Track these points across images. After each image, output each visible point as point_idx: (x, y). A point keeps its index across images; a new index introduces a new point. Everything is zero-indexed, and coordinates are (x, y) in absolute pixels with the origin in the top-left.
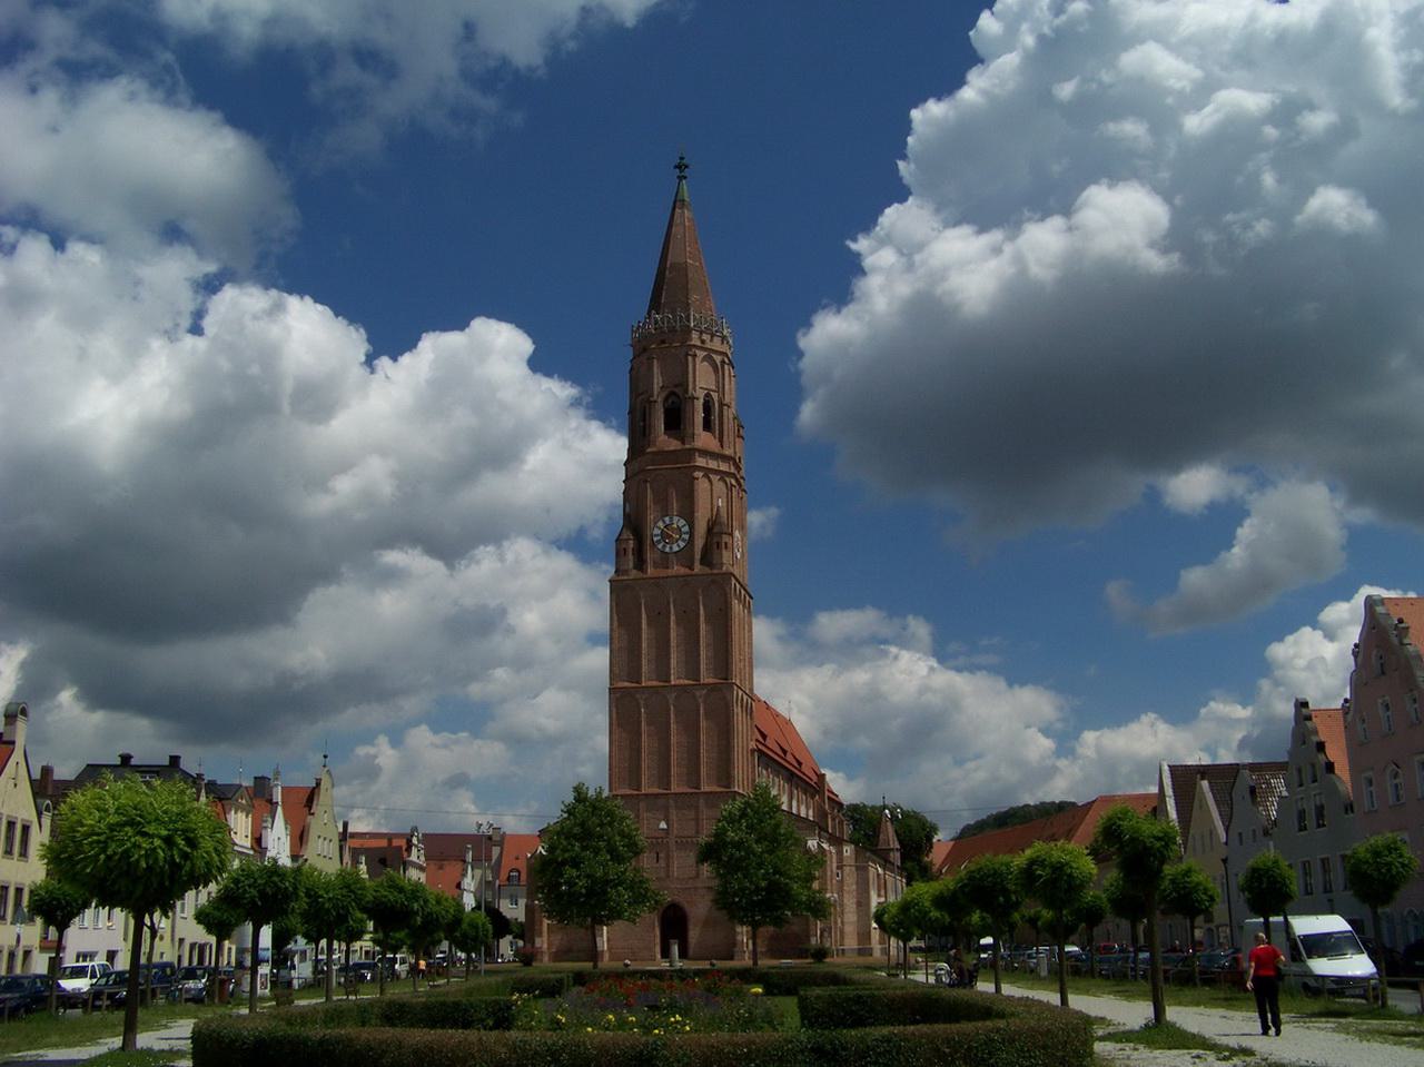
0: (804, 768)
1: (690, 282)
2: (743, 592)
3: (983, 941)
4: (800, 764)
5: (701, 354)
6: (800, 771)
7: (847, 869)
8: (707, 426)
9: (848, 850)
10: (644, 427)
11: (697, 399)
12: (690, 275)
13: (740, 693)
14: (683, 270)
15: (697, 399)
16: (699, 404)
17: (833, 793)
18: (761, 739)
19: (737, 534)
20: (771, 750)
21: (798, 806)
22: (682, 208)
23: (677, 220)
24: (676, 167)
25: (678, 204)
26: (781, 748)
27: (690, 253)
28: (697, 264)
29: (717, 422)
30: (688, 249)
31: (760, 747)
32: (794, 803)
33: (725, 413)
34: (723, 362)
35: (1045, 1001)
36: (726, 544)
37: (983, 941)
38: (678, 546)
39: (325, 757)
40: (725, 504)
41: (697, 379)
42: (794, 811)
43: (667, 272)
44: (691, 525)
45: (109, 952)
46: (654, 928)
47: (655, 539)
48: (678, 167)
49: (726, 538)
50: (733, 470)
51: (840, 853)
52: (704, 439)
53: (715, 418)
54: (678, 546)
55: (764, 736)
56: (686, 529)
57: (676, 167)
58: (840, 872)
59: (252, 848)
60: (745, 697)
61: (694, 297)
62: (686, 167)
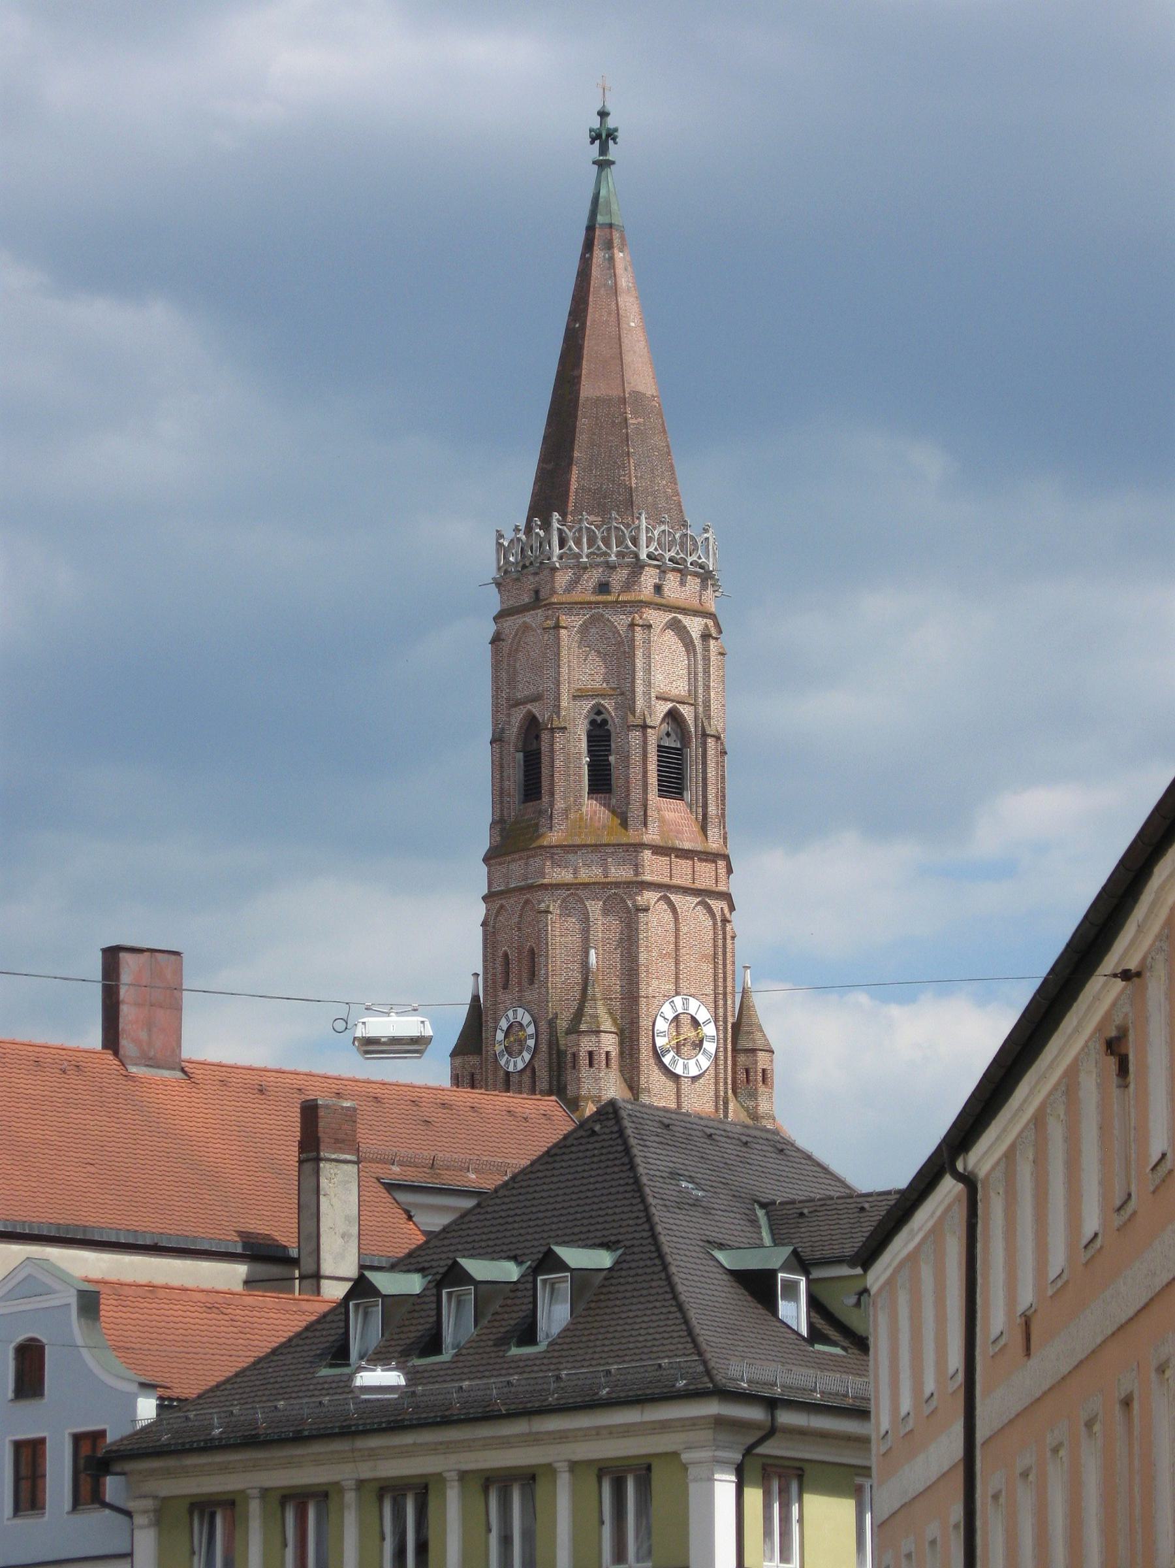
5: (658, 618)
47: (660, 1042)
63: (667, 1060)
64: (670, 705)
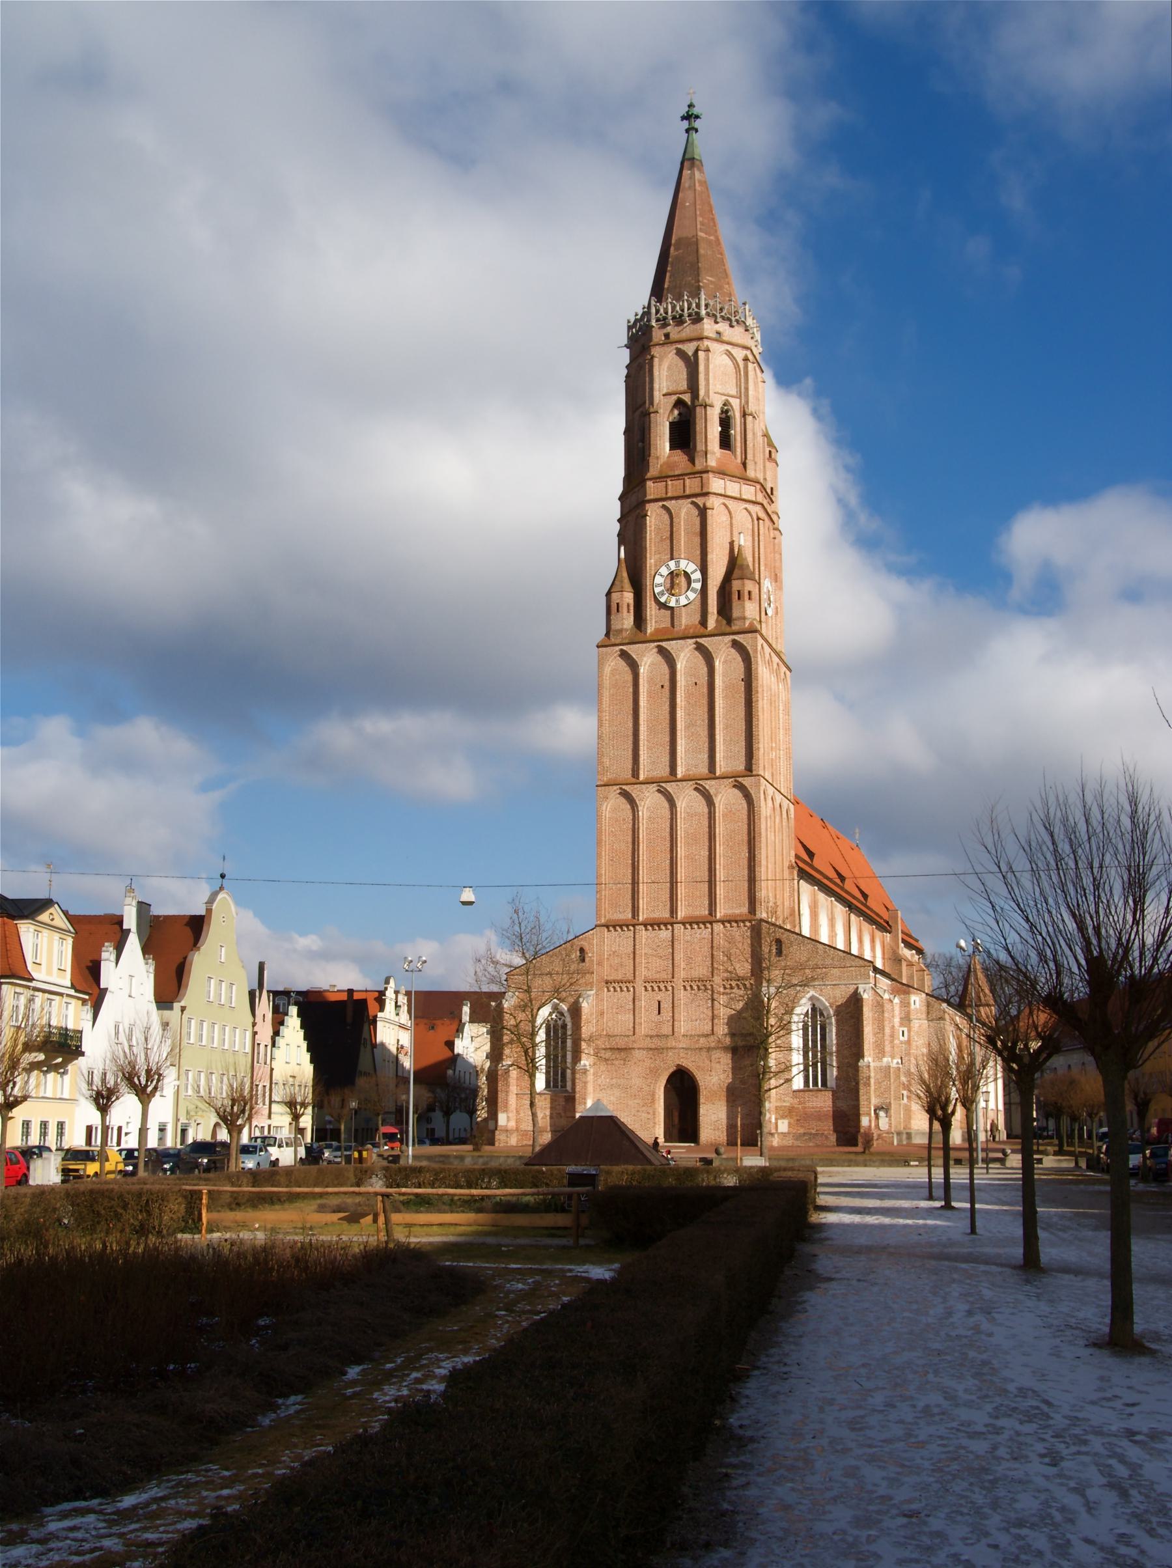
0: (870, 903)
1: (702, 259)
2: (776, 659)
3: (261, 1322)
4: (865, 896)
6: (842, 889)
7: (915, 1024)
8: (726, 442)
9: (917, 1001)
10: (644, 447)
11: (712, 406)
12: (702, 251)
13: (771, 790)
14: (692, 245)
15: (712, 406)
16: (714, 415)
17: (910, 936)
18: (806, 858)
19: (767, 584)
20: (877, 915)
21: (861, 941)
22: (692, 167)
23: (685, 183)
24: (683, 118)
25: (686, 164)
26: (836, 871)
27: (702, 224)
28: (712, 238)
29: (738, 438)
30: (699, 219)
31: (801, 864)
32: (823, 920)
33: (749, 426)
34: (746, 359)
35: (699, 518)
36: (749, 592)
37: (261, 1322)
38: (687, 597)
39: (223, 876)
40: (749, 544)
41: (711, 381)
42: (855, 951)
43: (672, 249)
44: (704, 570)
45: (88, 1127)
46: (653, 1101)
47: (657, 590)
48: (687, 117)
49: (749, 585)
50: (760, 498)
51: (905, 1004)
52: (714, 453)
53: (736, 432)
54: (687, 597)
55: (811, 854)
56: (697, 575)
57: (683, 118)
58: (905, 1029)
59: (73, 987)
60: (779, 797)
61: (706, 279)
62: (697, 117)
63: (663, 600)
64: (724, 398)
